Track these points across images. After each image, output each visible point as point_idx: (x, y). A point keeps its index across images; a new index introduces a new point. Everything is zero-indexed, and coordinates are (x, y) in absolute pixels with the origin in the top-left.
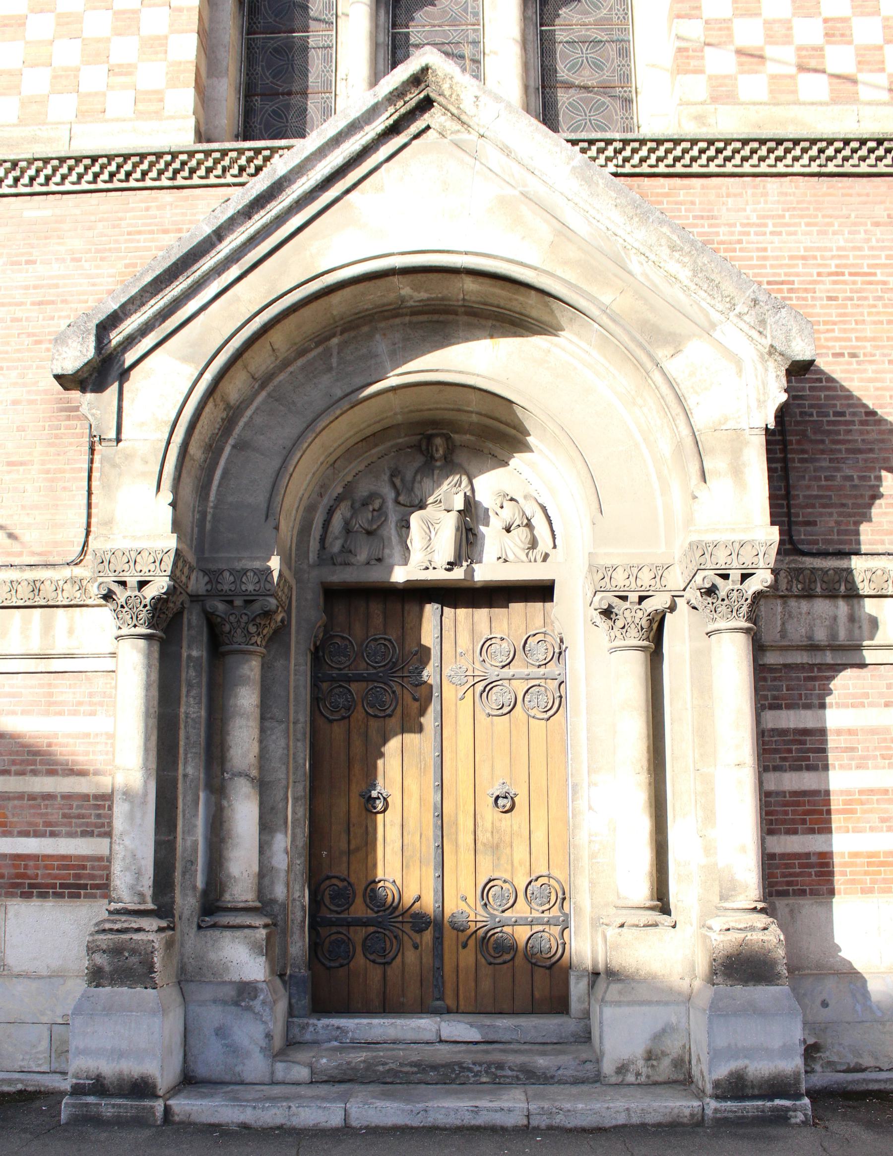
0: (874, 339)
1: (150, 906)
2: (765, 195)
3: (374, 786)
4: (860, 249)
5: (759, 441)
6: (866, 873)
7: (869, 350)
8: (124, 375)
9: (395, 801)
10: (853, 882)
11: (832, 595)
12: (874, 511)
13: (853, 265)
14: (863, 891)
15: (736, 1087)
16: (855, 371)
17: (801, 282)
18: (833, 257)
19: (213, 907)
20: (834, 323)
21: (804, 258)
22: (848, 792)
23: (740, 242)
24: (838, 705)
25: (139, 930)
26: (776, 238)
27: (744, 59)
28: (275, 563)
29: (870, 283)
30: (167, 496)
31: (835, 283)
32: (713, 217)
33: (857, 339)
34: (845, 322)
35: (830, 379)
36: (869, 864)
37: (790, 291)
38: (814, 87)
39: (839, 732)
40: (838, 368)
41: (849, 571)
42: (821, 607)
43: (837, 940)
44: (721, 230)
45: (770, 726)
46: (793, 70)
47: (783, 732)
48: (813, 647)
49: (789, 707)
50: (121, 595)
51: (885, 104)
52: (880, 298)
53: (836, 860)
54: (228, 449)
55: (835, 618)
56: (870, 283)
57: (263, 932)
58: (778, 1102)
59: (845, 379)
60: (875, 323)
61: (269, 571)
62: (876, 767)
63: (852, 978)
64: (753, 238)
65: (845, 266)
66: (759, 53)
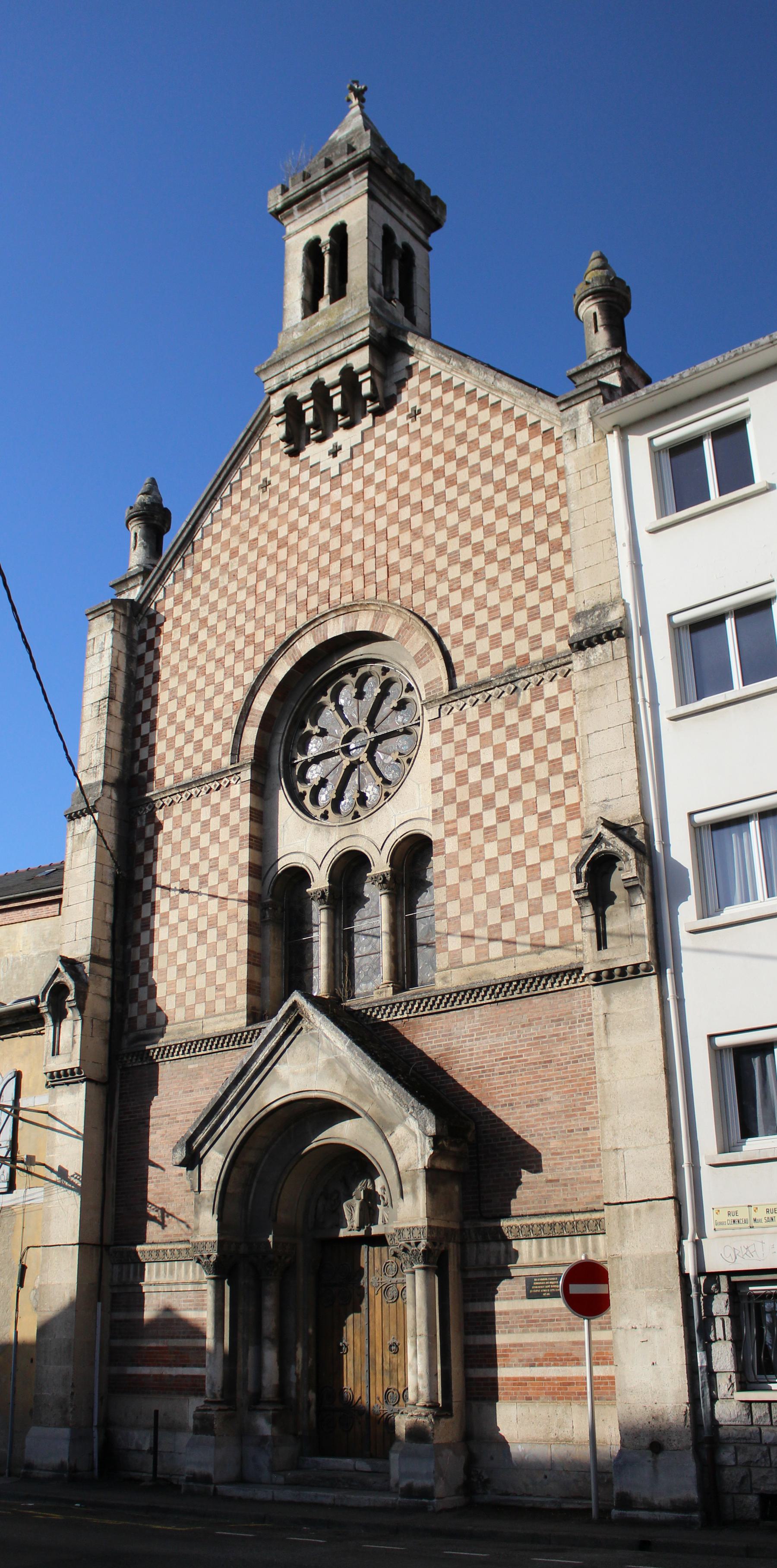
0: (520, 1094)
1: (219, 1399)
2: (473, 1017)
3: (342, 1341)
4: (515, 1042)
5: (422, 1176)
6: (513, 1389)
7: (518, 1100)
8: (200, 1161)
9: (351, 1347)
10: (506, 1393)
11: (498, 1241)
12: (518, 1192)
13: (512, 1052)
14: (511, 1399)
15: (409, 1491)
16: (511, 1114)
17: (488, 1066)
18: (502, 1049)
19: (256, 1400)
20: (502, 1087)
21: (490, 1052)
22: (505, 1345)
23: (461, 1047)
24: (501, 1299)
25: (210, 1410)
26: (478, 1042)
27: (465, 939)
28: (270, 1238)
29: (519, 1061)
30: (216, 1216)
31: (503, 1064)
32: (450, 1035)
33: (513, 1095)
34: (506, 1086)
35: (500, 1120)
36: (514, 1384)
37: (484, 1072)
38: (496, 950)
39: (501, 1313)
40: (503, 1113)
41: (500, 1227)
42: (493, 1246)
43: (498, 1425)
44: (454, 1041)
45: (471, 1310)
46: (486, 942)
47: (476, 1314)
48: (488, 1269)
49: (479, 1300)
50: (204, 1261)
51: (528, 953)
52: (524, 1070)
53: (499, 1382)
54: (255, 1184)
55: (499, 1252)
56: (519, 1061)
57: (271, 1412)
58: (424, 1500)
59: (506, 1119)
60: (520, 1085)
61: (269, 1242)
62: (517, 1332)
63: (503, 1444)
64: (468, 1043)
65: (508, 1054)
66: (470, 934)
